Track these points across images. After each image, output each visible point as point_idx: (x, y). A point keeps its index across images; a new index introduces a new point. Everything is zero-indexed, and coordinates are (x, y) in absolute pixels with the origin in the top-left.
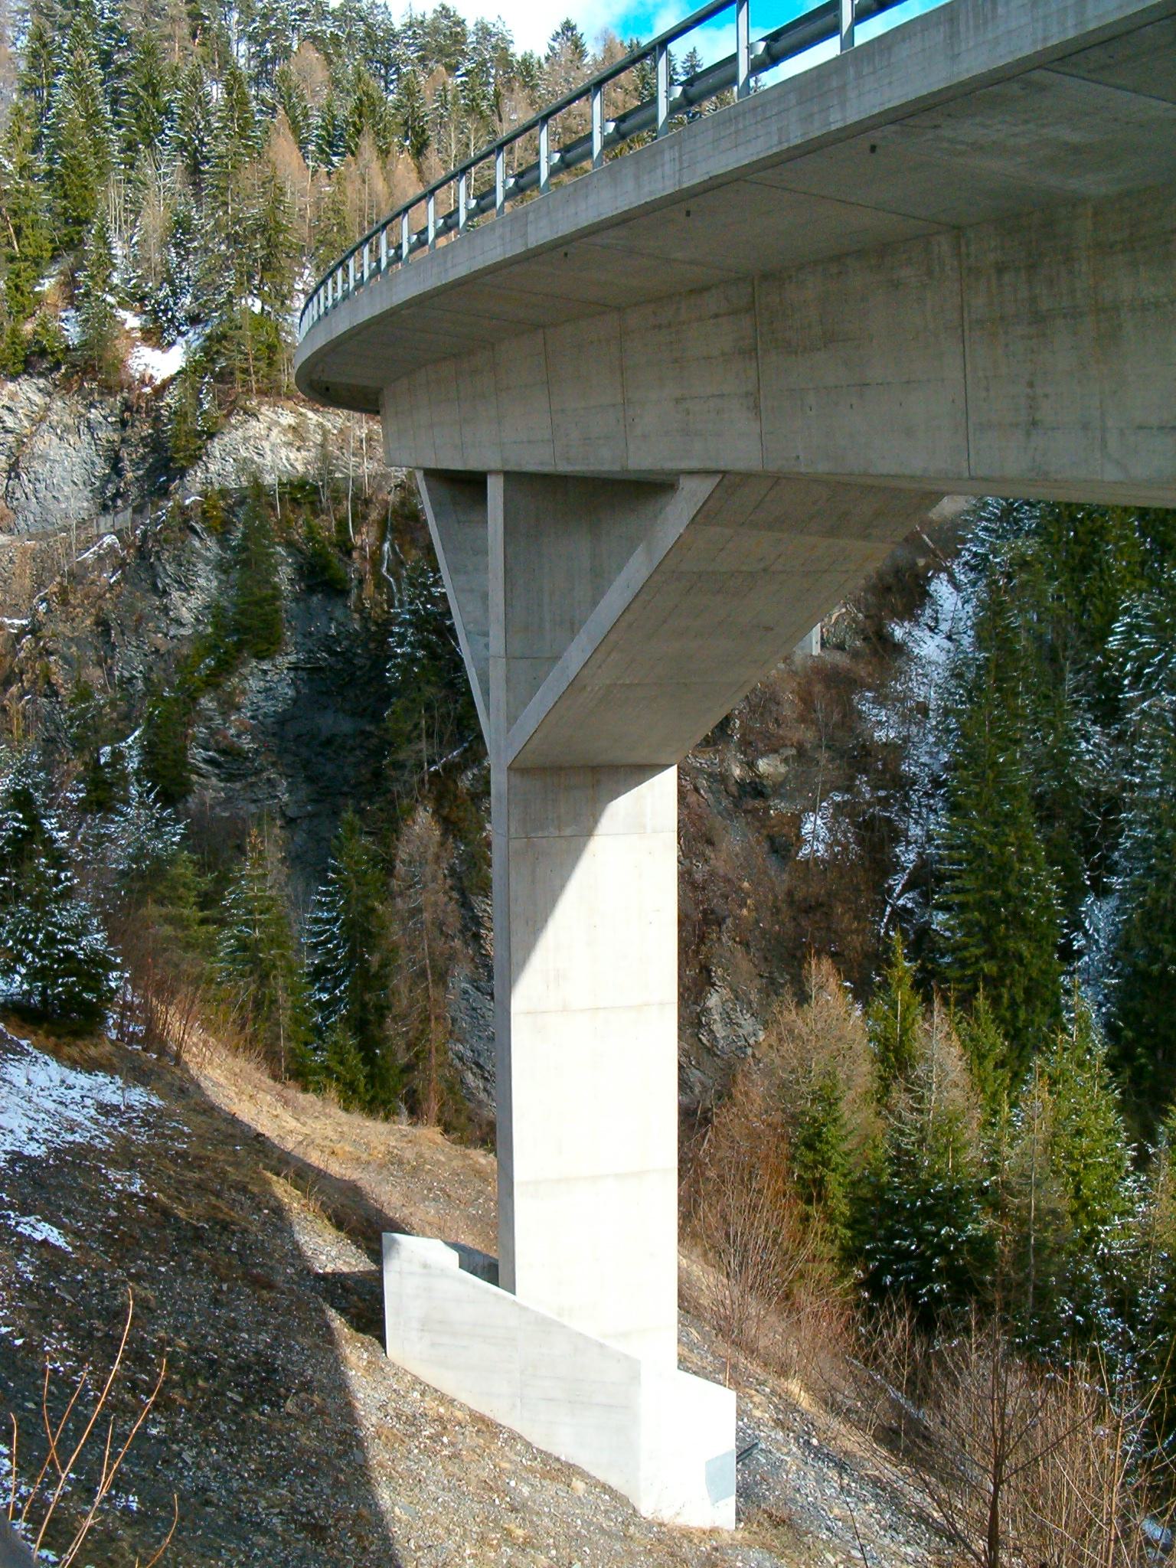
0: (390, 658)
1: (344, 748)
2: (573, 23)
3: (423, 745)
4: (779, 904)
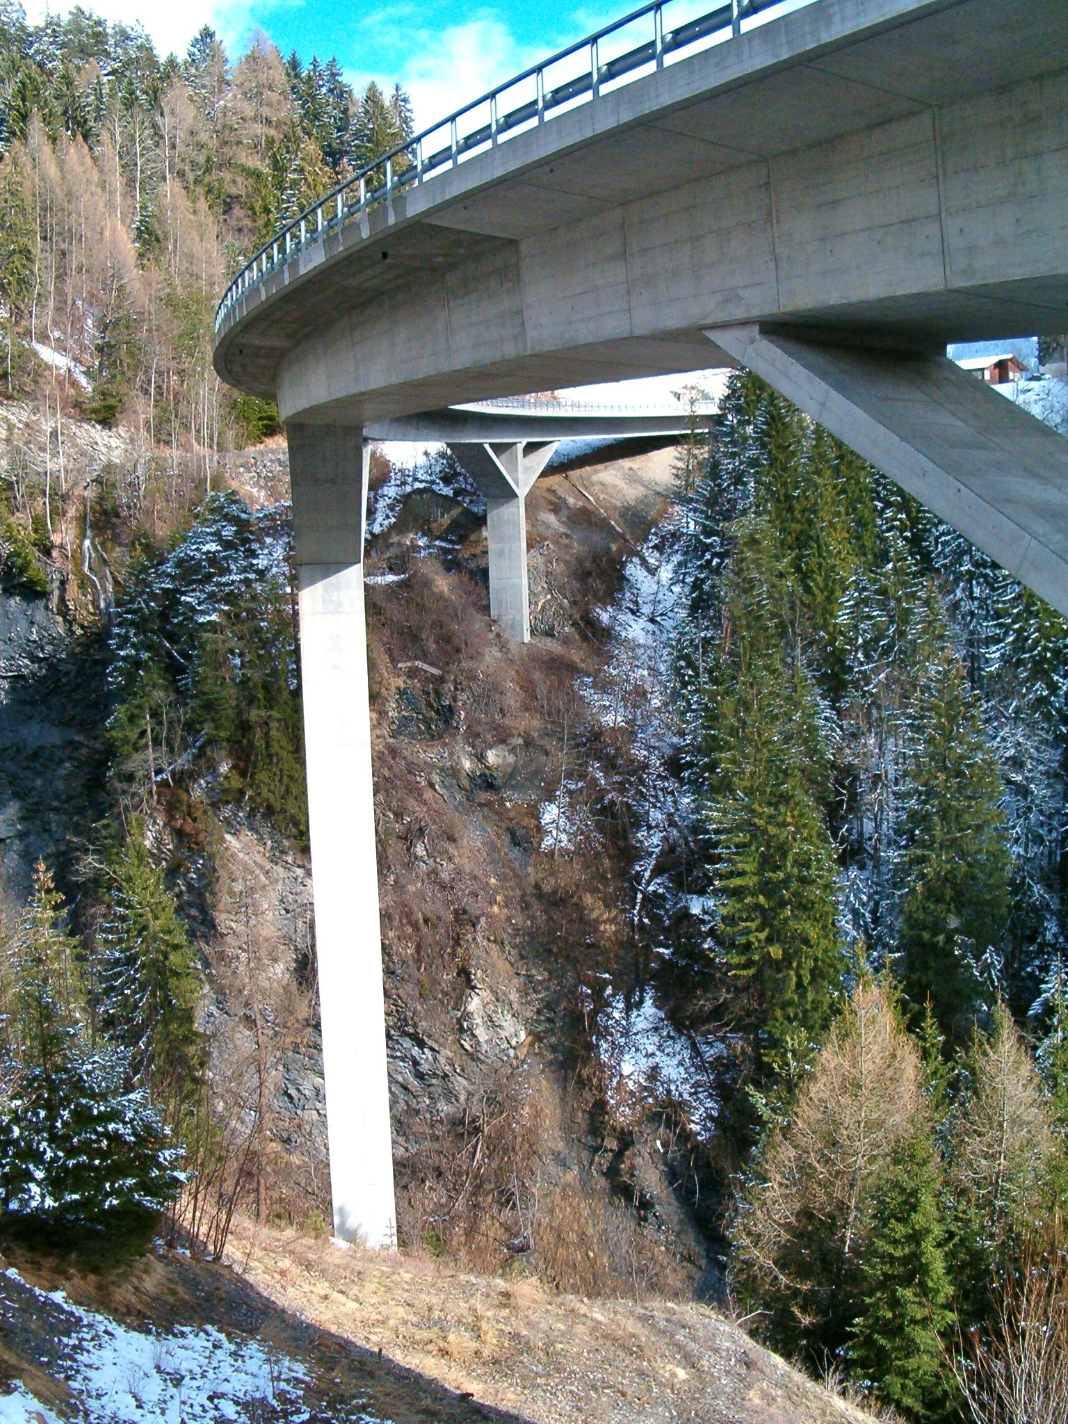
0: (110, 662)
1: (51, 760)
2: (212, 29)
3: (150, 754)
4: (528, 898)
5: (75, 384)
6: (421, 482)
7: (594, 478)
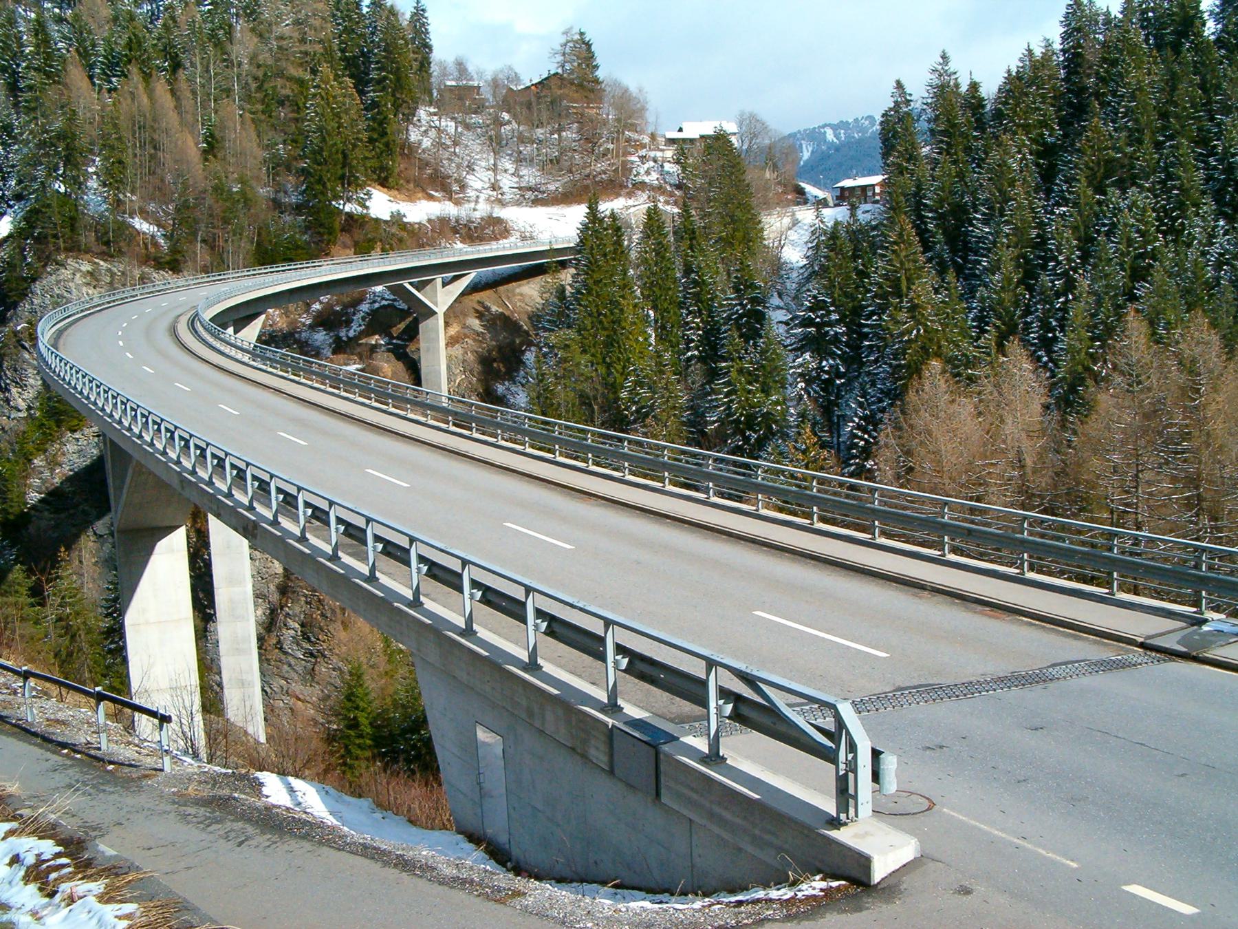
5: (156, 245)
6: (387, 300)
7: (518, 290)
